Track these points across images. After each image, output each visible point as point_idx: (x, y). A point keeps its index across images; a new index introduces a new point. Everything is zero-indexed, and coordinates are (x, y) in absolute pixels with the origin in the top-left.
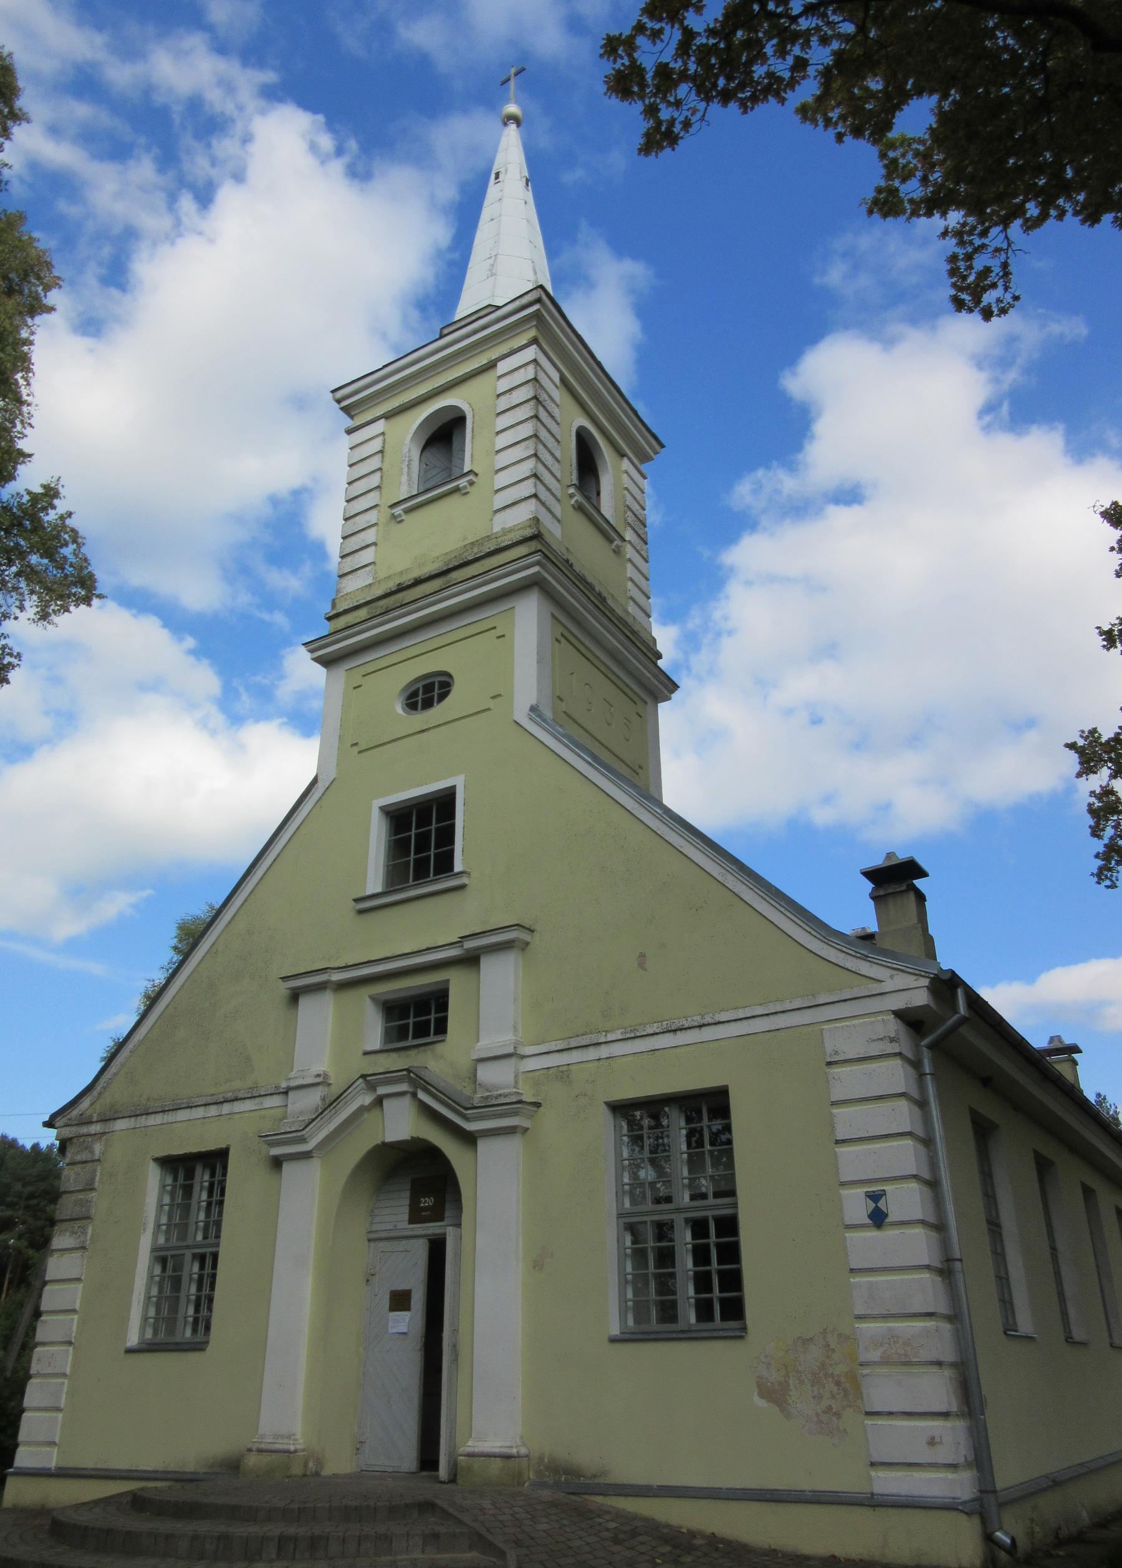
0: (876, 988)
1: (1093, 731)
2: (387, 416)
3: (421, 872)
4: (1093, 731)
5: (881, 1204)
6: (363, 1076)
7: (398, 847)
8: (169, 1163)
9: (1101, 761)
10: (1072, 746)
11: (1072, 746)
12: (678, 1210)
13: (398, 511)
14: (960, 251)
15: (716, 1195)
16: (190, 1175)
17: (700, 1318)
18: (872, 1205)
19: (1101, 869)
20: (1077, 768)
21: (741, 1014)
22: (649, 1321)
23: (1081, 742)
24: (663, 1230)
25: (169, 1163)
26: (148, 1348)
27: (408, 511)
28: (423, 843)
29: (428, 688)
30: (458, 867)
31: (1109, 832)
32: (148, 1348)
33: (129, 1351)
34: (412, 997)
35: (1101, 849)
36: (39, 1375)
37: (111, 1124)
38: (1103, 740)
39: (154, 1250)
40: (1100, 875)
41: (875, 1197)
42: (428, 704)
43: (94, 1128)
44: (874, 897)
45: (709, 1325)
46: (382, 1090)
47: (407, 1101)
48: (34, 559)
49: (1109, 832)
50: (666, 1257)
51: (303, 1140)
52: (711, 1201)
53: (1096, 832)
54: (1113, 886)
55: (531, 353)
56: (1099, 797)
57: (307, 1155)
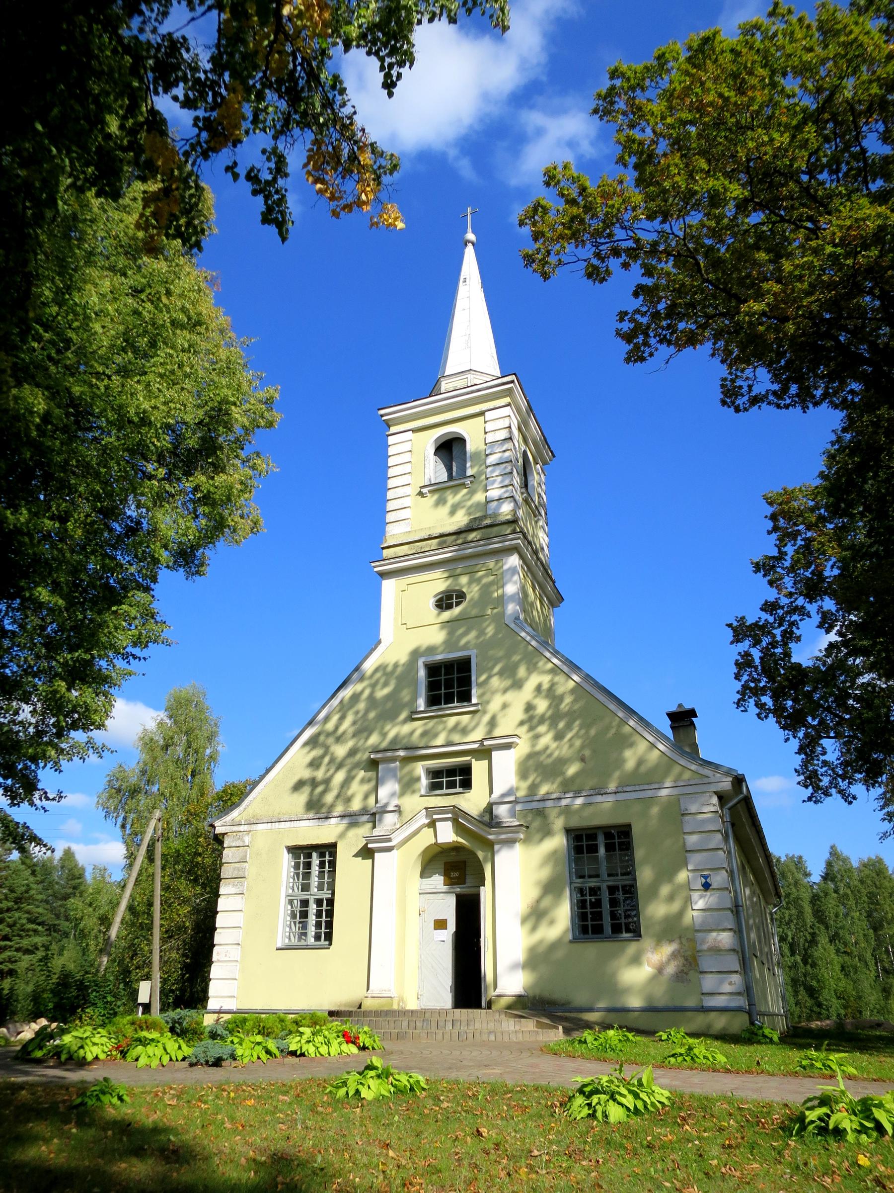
0: (706, 780)
1: (743, 618)
2: (414, 431)
4: (743, 618)
6: (426, 809)
8: (294, 850)
9: (746, 636)
10: (730, 625)
11: (730, 625)
12: (603, 881)
13: (425, 490)
14: (729, 377)
15: (623, 874)
16: (309, 856)
19: (739, 700)
20: (732, 638)
21: (637, 788)
23: (735, 624)
24: (305, 903)
25: (294, 850)
29: (450, 597)
30: (474, 700)
31: (745, 678)
35: (739, 688)
36: (218, 961)
38: (748, 624)
39: (287, 896)
40: (738, 704)
41: (706, 877)
43: (242, 828)
44: (672, 728)
46: (435, 817)
47: (449, 824)
49: (745, 678)
51: (390, 840)
52: (620, 877)
53: (737, 677)
54: (746, 711)
55: (507, 411)
56: (742, 657)
57: (389, 849)
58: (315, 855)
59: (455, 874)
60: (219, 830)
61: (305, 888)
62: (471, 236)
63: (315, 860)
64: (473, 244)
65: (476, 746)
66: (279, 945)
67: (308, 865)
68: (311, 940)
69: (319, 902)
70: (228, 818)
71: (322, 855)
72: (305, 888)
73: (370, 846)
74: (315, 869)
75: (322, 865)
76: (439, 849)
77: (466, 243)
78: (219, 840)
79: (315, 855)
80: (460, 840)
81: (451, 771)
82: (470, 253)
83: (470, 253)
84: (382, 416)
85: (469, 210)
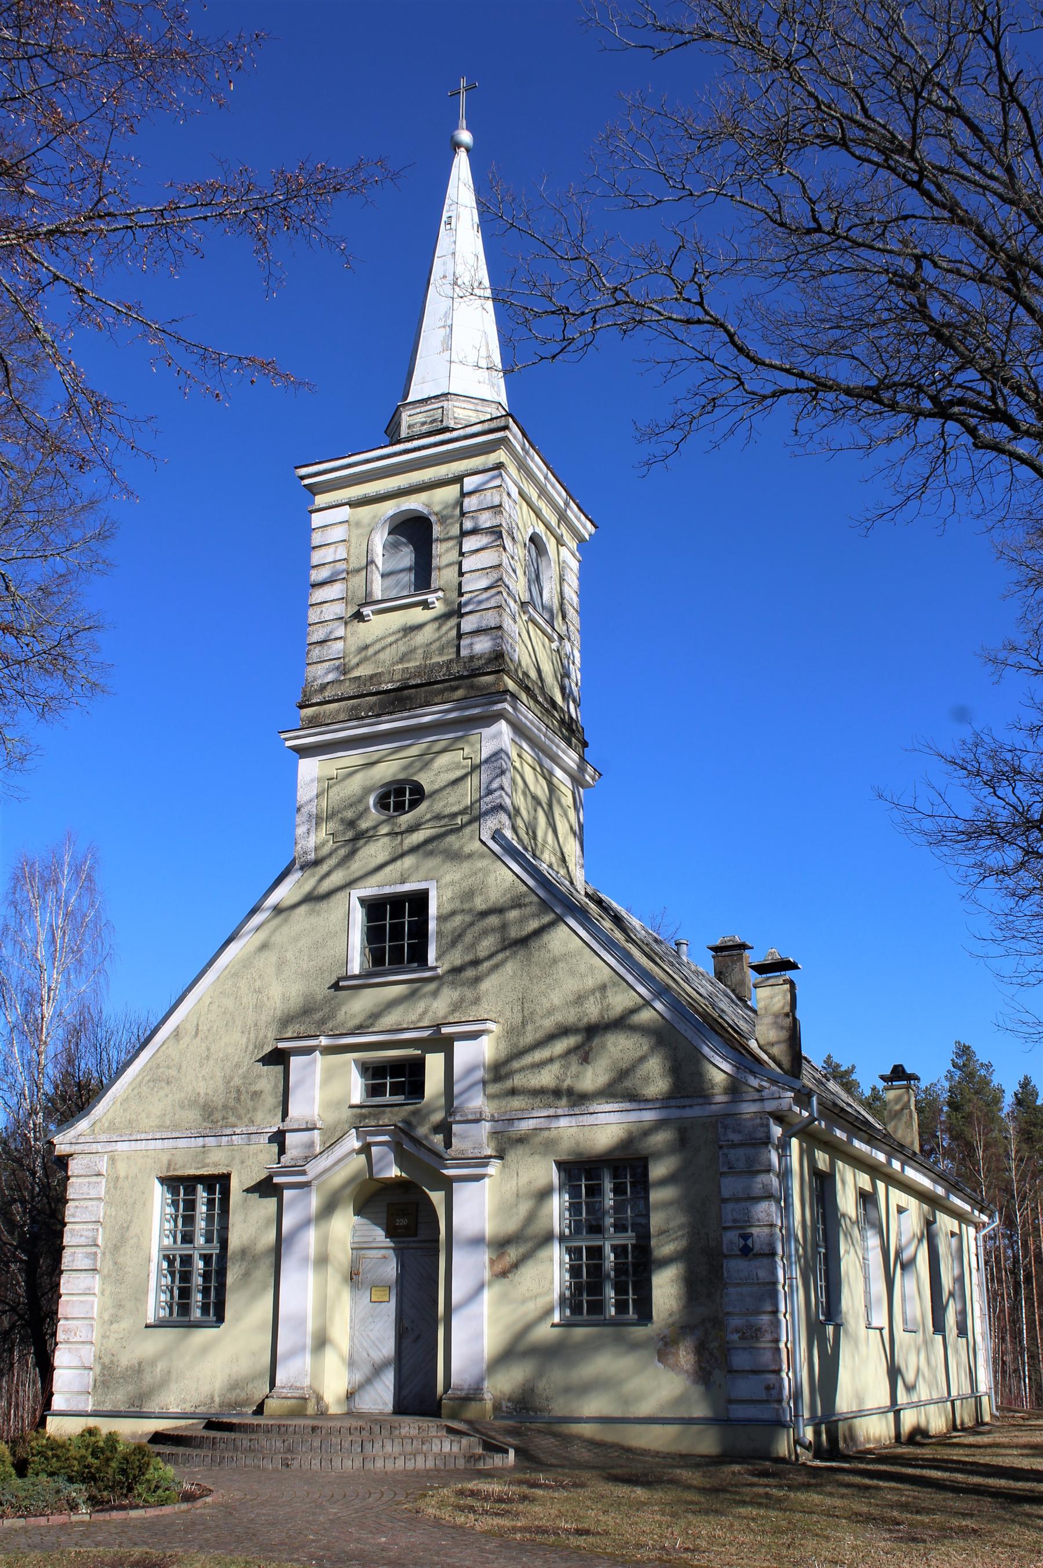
3: (397, 958)
5: (749, 1242)
7: (373, 935)
16: (191, 1191)
17: (203, 1314)
18: (742, 1242)
22: (581, 1313)
24: (187, 1260)
25: (172, 1182)
26: (160, 1324)
27: (375, 613)
28: (397, 932)
29: (400, 792)
32: (160, 1324)
33: (147, 1326)
34: (373, 1063)
37: (554, 1121)
42: (400, 807)
45: (578, 1318)
46: (370, 1139)
48: (989, 344)
50: (186, 1277)
58: (200, 1187)
59: (402, 1222)
60: (61, 1149)
61: (188, 1238)
62: (465, 136)
63: (201, 1194)
64: (468, 150)
65: (426, 1034)
66: (151, 1320)
67: (191, 1205)
68: (197, 1314)
69: (206, 1258)
70: (71, 1134)
71: (210, 1190)
72: (188, 1238)
73: (276, 1180)
74: (202, 1209)
75: (210, 1203)
76: (379, 1185)
77: (457, 145)
78: (63, 1162)
79: (200, 1187)
80: (404, 1175)
81: (396, 1068)
82: (461, 167)
83: (461, 167)
84: (302, 478)
85: (463, 83)
